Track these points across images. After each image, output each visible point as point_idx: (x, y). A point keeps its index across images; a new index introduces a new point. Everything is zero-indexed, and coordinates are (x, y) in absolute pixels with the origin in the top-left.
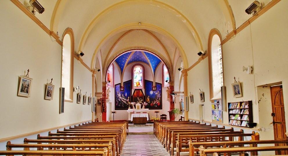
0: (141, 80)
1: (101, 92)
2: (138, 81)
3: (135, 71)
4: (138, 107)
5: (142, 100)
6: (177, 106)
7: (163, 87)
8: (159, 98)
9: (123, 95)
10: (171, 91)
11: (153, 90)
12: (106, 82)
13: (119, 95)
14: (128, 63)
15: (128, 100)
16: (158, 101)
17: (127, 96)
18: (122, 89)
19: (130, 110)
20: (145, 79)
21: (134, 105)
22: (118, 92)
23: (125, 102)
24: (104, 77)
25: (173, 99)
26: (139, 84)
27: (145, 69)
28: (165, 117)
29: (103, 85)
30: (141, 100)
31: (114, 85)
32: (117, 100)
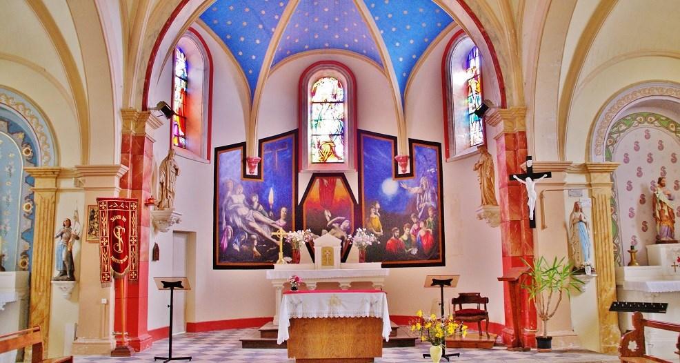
0: (343, 135)
1: (109, 163)
2: (328, 139)
3: (313, 94)
4: (324, 257)
5: (346, 224)
6: (548, 249)
7: (448, 156)
8: (430, 213)
9: (255, 199)
10: (512, 164)
11: (397, 176)
12: (145, 107)
13: (234, 197)
14: (280, 59)
15: (282, 222)
16: (422, 224)
17: (279, 204)
18: (252, 168)
19: (284, 268)
20: (361, 127)
21: (307, 244)
22: (231, 185)
23: (268, 234)
24: (137, 85)
25: (532, 204)
26: (333, 152)
27: (359, 79)
28: (474, 306)
29: (126, 127)
30: (340, 222)
31: (214, 145)
32: (227, 220)
